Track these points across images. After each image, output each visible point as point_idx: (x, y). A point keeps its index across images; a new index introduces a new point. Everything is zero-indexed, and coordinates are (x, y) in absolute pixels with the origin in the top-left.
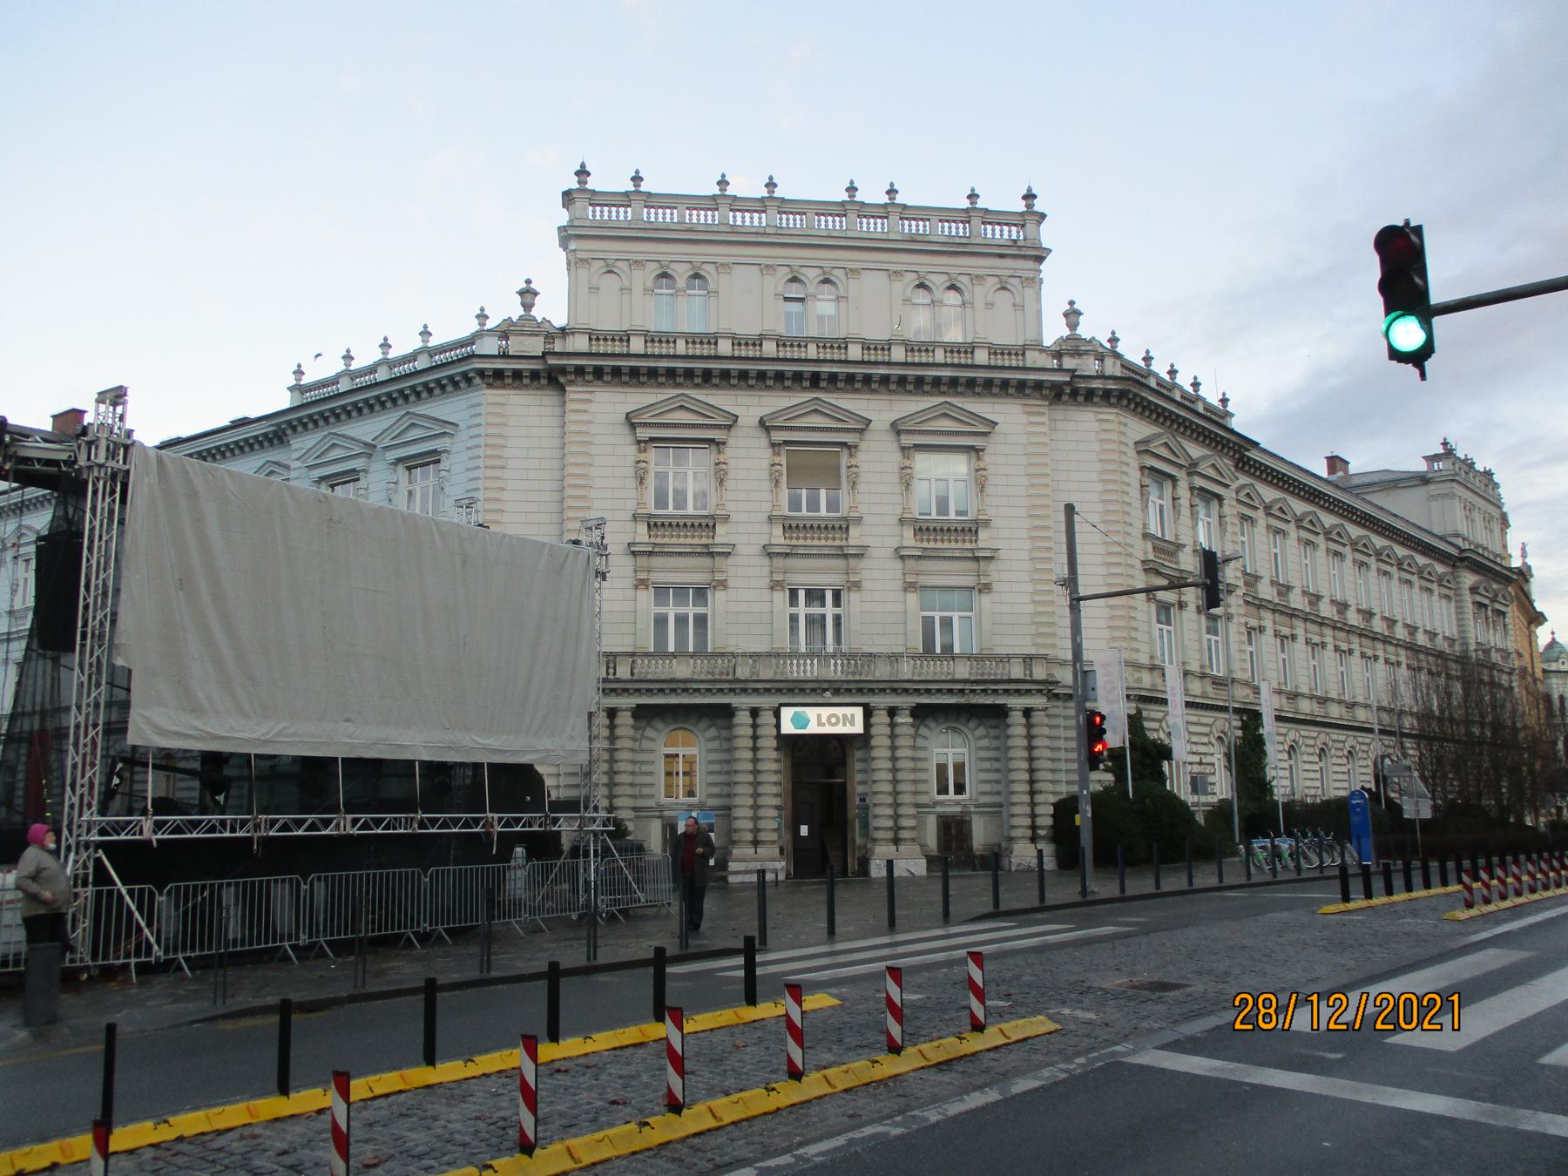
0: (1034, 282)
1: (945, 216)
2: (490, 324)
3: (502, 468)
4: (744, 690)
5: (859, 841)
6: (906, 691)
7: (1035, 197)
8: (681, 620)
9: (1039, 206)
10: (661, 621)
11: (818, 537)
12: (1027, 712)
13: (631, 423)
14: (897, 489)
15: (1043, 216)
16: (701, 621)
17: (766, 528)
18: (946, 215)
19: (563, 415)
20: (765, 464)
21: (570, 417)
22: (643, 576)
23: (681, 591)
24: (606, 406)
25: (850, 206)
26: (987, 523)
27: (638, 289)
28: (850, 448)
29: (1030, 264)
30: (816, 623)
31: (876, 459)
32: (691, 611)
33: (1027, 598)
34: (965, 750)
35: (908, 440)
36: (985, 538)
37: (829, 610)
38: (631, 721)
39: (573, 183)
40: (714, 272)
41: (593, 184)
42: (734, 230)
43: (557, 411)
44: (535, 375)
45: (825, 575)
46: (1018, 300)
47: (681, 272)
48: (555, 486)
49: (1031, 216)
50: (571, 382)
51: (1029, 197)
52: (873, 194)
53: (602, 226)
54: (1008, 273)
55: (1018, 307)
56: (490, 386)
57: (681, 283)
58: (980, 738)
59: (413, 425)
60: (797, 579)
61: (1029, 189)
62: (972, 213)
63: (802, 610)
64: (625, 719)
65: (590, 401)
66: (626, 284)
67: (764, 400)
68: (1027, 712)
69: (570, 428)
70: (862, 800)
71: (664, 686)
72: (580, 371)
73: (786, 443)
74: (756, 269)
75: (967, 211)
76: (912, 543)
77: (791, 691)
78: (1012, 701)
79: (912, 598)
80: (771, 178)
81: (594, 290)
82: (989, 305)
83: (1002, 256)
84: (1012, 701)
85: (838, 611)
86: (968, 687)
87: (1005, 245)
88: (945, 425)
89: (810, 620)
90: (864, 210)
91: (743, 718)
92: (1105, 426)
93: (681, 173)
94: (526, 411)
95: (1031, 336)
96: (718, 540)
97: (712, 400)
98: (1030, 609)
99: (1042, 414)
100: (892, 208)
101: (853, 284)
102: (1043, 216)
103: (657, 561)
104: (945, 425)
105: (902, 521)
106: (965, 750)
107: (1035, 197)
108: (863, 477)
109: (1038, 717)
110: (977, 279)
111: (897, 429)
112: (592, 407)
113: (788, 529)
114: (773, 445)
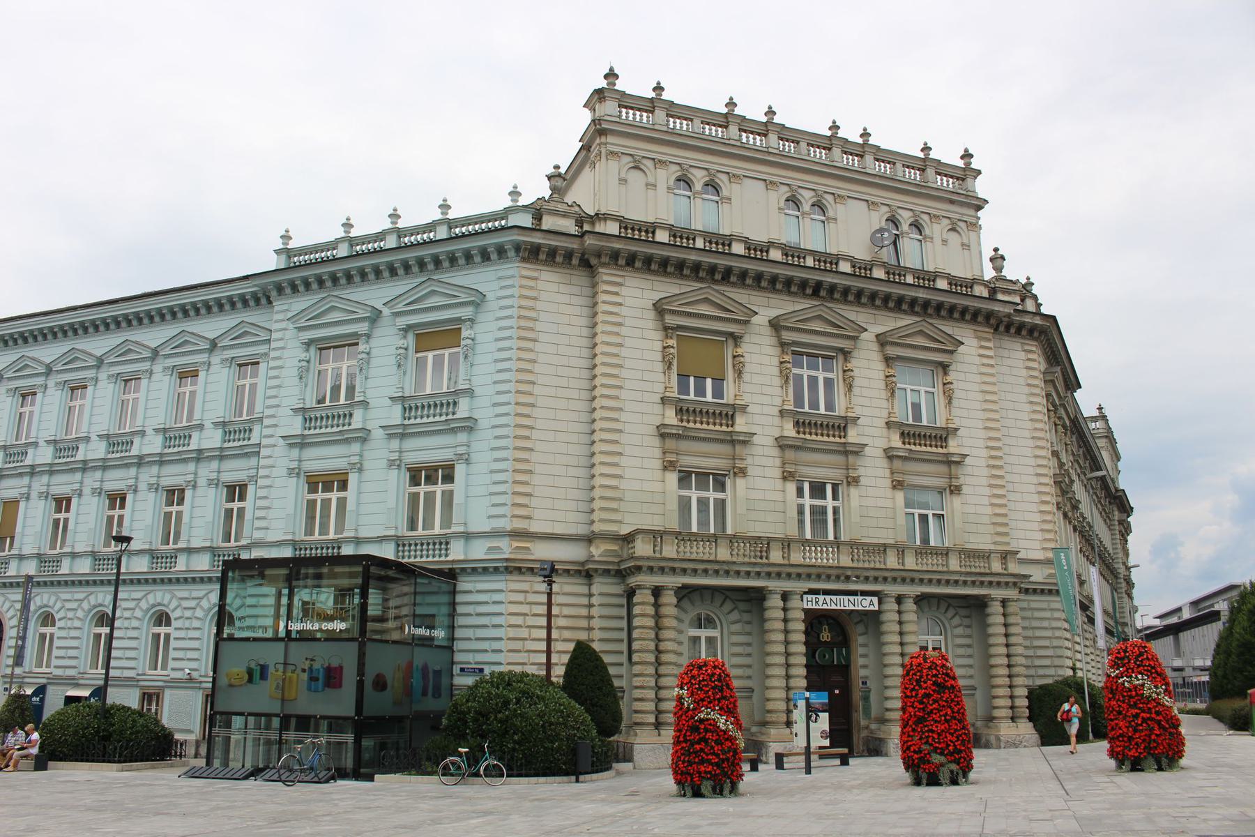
0: (975, 226)
1: (708, 118)
2: (523, 201)
3: (535, 340)
4: (779, 575)
5: (863, 723)
6: (673, 570)
7: (971, 156)
8: (703, 503)
9: (975, 164)
10: (684, 505)
11: (819, 432)
12: (1004, 602)
13: (660, 309)
14: (884, 394)
15: (979, 172)
16: (721, 505)
17: (777, 421)
18: (708, 117)
19: (595, 295)
20: (775, 361)
21: (602, 297)
22: (672, 458)
23: (702, 476)
24: (634, 297)
25: (831, 141)
26: (743, 409)
27: (662, 187)
28: (736, 339)
29: (972, 212)
30: (819, 513)
31: (867, 364)
32: (712, 495)
33: (986, 501)
34: (942, 638)
35: (891, 351)
36: (953, 446)
37: (829, 503)
38: (914, 607)
39: (603, 84)
40: (832, 202)
41: (620, 85)
42: (672, 132)
43: (587, 291)
44: (569, 255)
45: (824, 469)
46: (966, 241)
47: (699, 178)
48: (585, 363)
49: (966, 173)
50: (605, 265)
51: (967, 156)
52: (851, 133)
53: (622, 122)
54: (958, 216)
55: (966, 246)
56: (524, 260)
57: (698, 186)
58: (733, 623)
59: (433, 291)
60: (689, 461)
61: (966, 150)
62: (924, 163)
63: (807, 501)
64: (669, 598)
65: (621, 284)
66: (651, 180)
67: (657, 285)
68: (1004, 602)
69: (602, 307)
70: (864, 683)
71: (677, 565)
72: (615, 255)
73: (680, 328)
74: (762, 184)
75: (652, 100)
76: (675, 421)
77: (819, 577)
78: (772, 584)
79: (900, 496)
80: (865, 129)
81: (623, 181)
82: (945, 242)
83: (952, 202)
84: (772, 584)
85: (836, 504)
86: (701, 566)
87: (948, 190)
88: (920, 341)
89: (814, 510)
90: (746, 125)
91: (775, 602)
92: (1030, 356)
93: (696, 89)
94: (555, 292)
95: (977, 273)
96: (737, 428)
97: (852, 316)
98: (989, 510)
99: (989, 340)
100: (863, 148)
101: (840, 208)
102: (979, 172)
103: (684, 445)
104: (920, 341)
105: (889, 425)
106: (942, 638)
107: (971, 156)
108: (748, 368)
109: (1012, 608)
110: (934, 218)
111: (882, 340)
112: (540, 285)
113: (680, 411)
114: (666, 329)
